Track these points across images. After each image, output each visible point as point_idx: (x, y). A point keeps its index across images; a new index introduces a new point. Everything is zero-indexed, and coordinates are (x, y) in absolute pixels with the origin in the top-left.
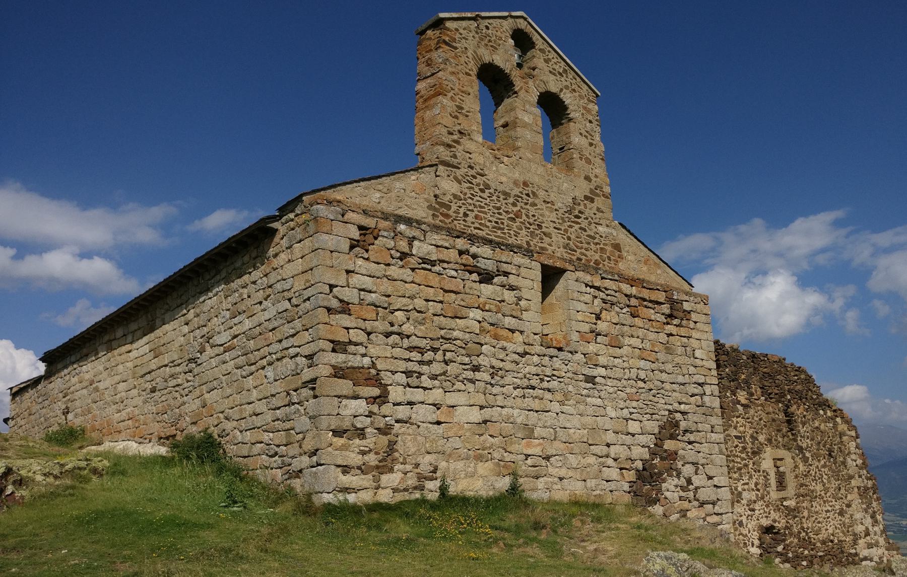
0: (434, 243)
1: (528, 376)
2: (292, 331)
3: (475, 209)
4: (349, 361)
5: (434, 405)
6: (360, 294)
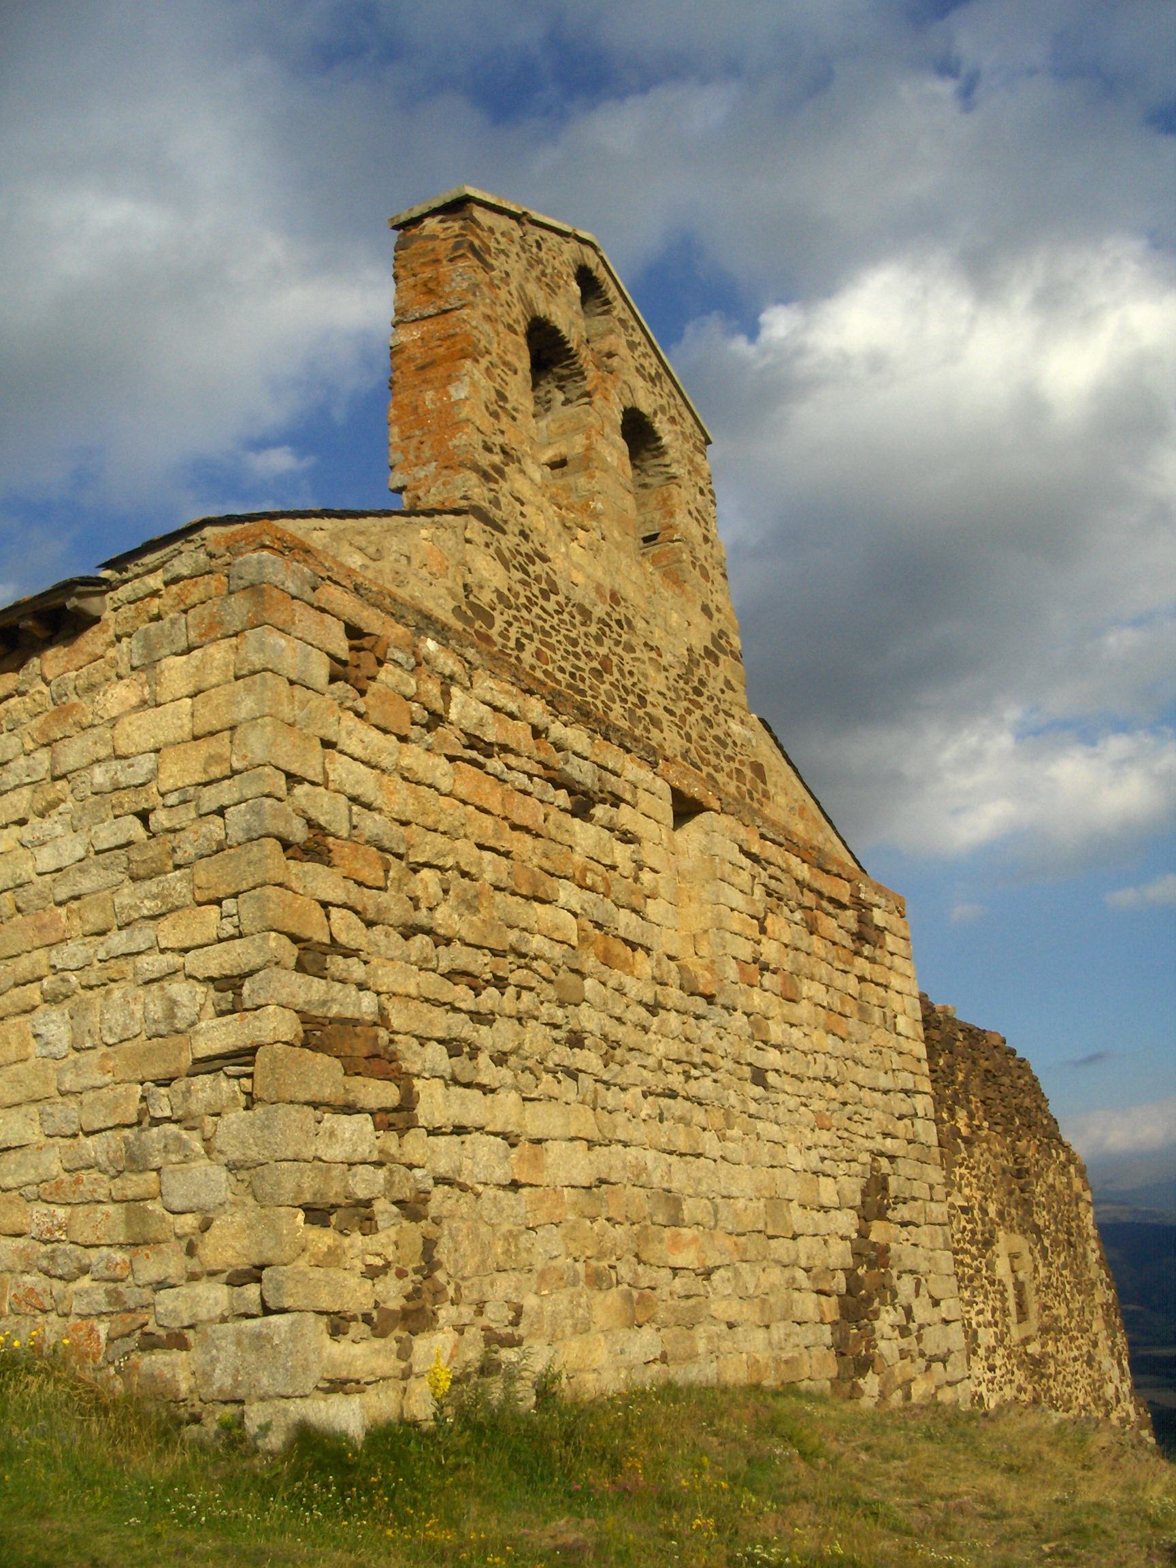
0: (488, 698)
1: (665, 1063)
2: (149, 906)
3: (535, 635)
4: (334, 1000)
5: (505, 1136)
6: (350, 810)
